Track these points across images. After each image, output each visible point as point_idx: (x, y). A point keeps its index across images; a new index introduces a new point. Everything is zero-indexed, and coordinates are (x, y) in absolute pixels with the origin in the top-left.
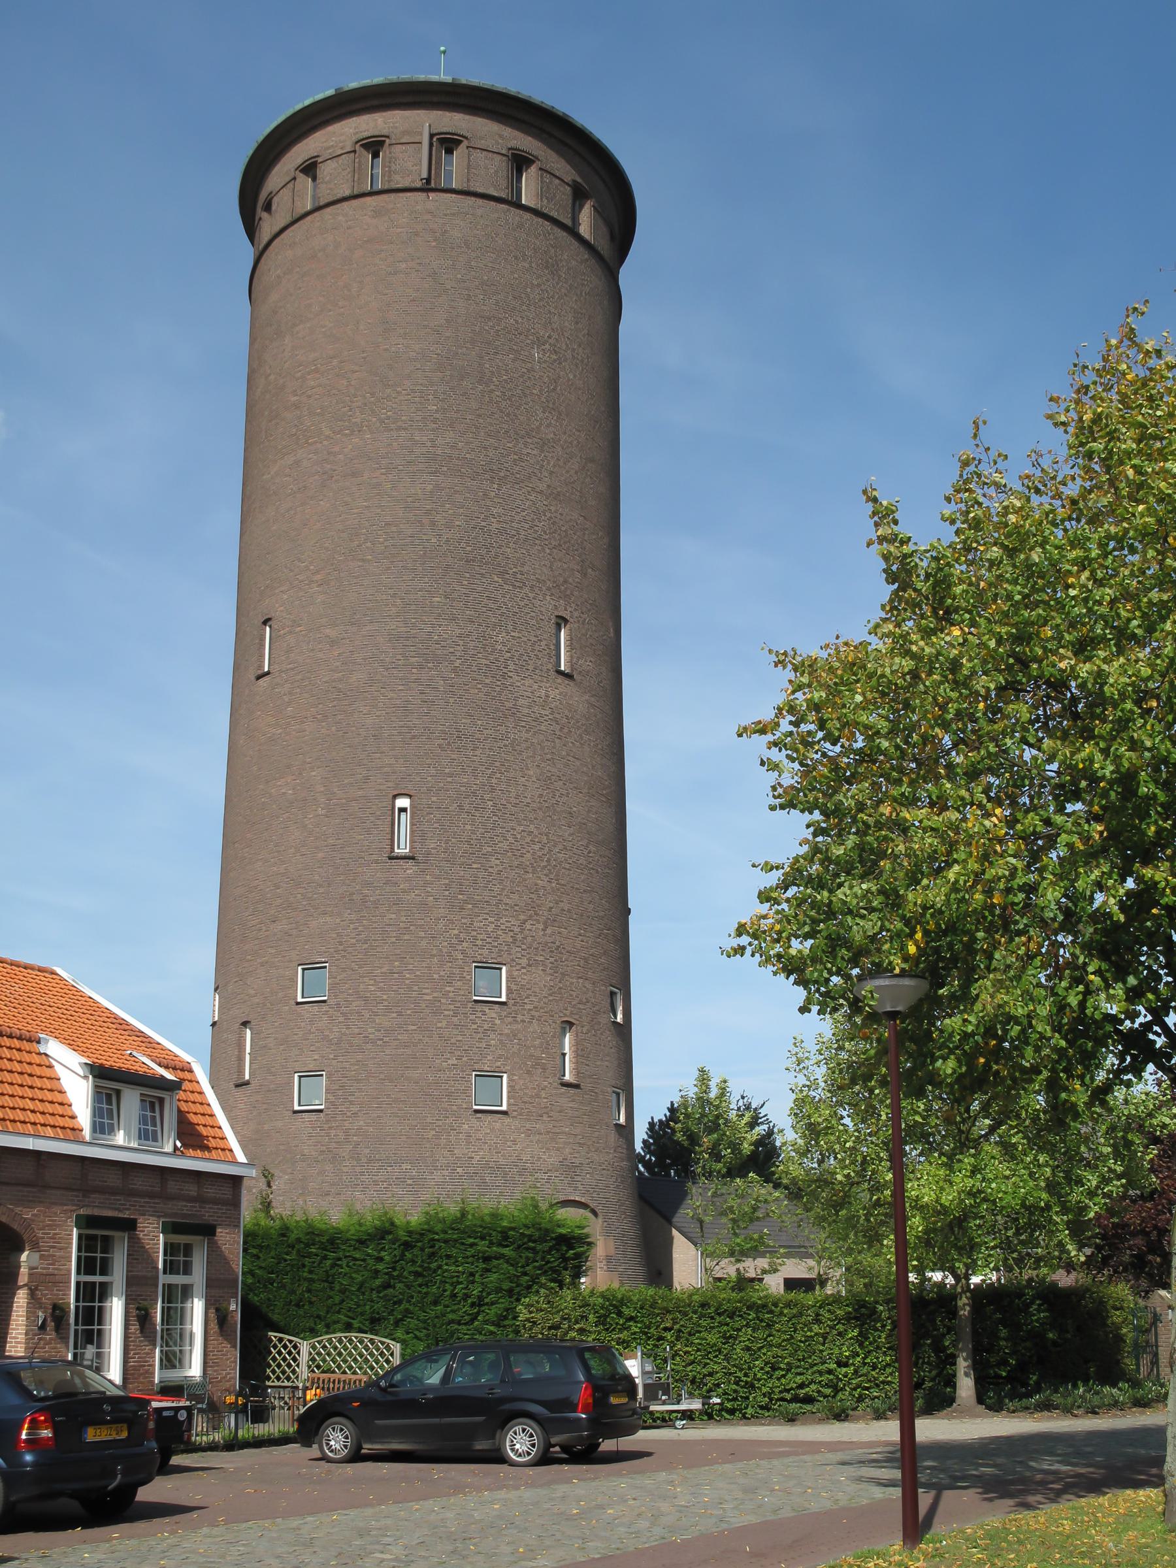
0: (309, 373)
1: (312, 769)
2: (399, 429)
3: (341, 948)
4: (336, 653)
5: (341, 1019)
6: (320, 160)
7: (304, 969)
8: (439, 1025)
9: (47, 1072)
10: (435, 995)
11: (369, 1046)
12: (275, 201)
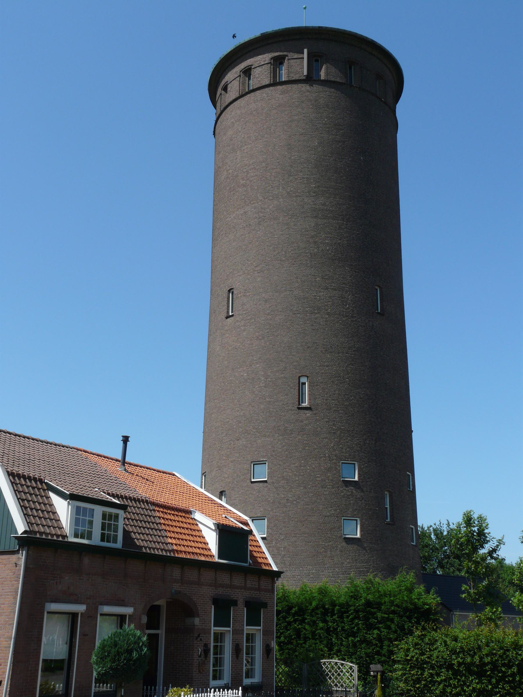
0: (250, 169)
1: (257, 363)
2: (297, 196)
3: (274, 453)
4: (268, 306)
5: (274, 490)
6: (253, 67)
7: (254, 465)
8: (325, 493)
9: (195, 527)
10: (322, 477)
11: (289, 504)
12: (229, 86)
